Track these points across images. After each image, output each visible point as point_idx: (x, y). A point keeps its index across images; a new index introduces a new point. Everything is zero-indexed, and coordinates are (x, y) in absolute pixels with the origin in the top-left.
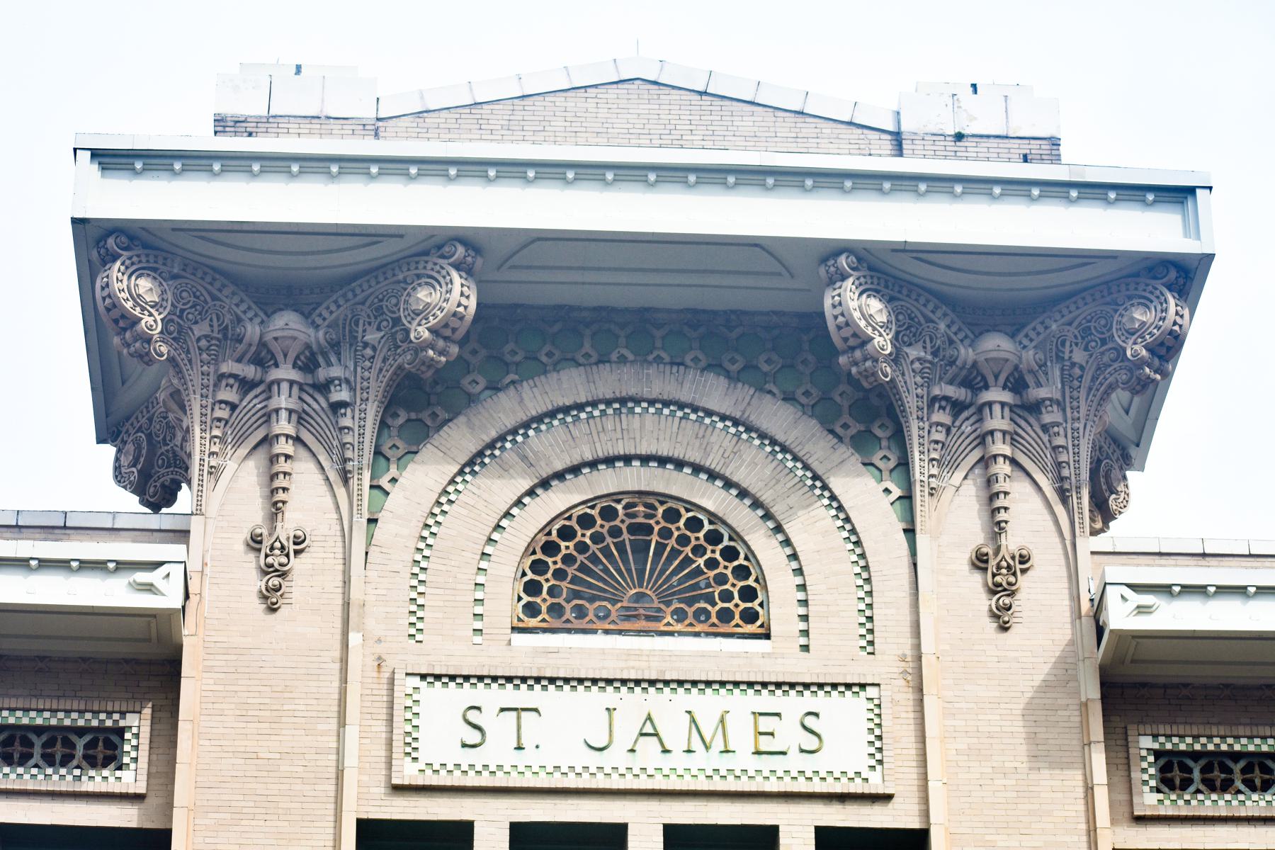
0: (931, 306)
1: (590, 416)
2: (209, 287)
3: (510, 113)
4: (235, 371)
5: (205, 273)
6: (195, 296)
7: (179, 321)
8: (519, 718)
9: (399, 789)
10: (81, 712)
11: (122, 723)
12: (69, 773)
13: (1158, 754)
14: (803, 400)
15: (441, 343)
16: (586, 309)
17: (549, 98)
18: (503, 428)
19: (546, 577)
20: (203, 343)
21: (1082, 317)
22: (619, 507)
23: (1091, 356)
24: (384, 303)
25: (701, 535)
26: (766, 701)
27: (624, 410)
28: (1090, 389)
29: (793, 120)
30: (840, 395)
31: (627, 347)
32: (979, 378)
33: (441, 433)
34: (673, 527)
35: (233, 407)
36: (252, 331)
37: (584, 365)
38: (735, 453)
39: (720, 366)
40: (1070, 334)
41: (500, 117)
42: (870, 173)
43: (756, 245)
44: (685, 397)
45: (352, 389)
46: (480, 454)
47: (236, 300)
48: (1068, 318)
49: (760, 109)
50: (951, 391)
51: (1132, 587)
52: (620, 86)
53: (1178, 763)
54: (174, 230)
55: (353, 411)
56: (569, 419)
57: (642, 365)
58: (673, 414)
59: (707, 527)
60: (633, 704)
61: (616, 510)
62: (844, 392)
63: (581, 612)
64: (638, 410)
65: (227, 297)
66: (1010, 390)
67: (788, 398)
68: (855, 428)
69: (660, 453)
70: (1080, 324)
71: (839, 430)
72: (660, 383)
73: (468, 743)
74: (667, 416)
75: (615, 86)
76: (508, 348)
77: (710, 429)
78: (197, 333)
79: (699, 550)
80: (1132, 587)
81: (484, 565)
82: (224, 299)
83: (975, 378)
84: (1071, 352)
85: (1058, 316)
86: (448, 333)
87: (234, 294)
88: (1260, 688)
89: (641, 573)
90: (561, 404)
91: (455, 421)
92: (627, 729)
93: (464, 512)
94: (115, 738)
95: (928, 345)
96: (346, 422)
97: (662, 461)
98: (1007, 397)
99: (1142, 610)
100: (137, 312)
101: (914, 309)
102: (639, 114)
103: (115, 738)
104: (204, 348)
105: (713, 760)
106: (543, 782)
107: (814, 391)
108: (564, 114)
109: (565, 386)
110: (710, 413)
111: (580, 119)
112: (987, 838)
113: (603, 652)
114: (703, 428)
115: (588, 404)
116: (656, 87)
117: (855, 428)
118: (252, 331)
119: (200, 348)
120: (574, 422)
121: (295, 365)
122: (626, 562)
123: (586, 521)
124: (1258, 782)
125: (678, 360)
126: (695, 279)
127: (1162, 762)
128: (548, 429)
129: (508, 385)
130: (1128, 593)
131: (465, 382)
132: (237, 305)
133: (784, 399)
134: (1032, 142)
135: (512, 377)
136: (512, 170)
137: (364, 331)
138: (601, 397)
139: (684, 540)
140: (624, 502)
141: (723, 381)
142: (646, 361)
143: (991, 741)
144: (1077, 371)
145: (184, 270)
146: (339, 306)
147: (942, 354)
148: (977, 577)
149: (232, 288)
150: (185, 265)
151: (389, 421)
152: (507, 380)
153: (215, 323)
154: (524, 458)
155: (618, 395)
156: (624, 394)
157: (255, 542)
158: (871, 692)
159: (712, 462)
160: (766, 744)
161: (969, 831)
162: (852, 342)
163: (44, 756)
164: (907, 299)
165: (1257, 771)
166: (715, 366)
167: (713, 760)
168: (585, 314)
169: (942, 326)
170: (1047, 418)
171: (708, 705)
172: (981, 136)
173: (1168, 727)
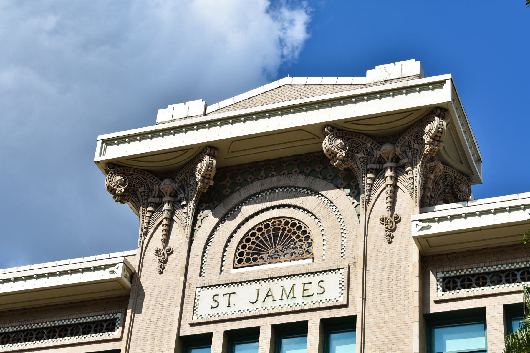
0: (364, 139)
1: (262, 195)
2: (143, 176)
3: (245, 104)
5: (141, 172)
6: (138, 179)
7: (133, 188)
8: (230, 296)
9: (192, 325)
11: (116, 317)
14: (329, 178)
16: (262, 161)
17: (257, 97)
18: (234, 204)
19: (246, 250)
20: (142, 194)
21: (415, 132)
23: (419, 145)
24: (448, 178)
26: (307, 279)
27: (273, 192)
28: (420, 156)
29: (333, 88)
30: (341, 174)
31: (275, 171)
32: (383, 160)
33: (215, 209)
34: (287, 227)
37: (261, 180)
38: (306, 199)
39: (303, 172)
40: (412, 139)
41: (242, 106)
42: (326, 100)
43: (300, 130)
44: (291, 184)
47: (152, 178)
48: (410, 134)
49: (323, 86)
50: (374, 166)
51: (420, 221)
52: (279, 88)
53: (467, 279)
55: (187, 207)
56: (255, 198)
57: (279, 176)
60: (264, 286)
61: (269, 224)
62: (342, 173)
64: (277, 191)
65: (149, 178)
66: (395, 162)
69: (282, 204)
70: (414, 135)
72: (284, 181)
73: (213, 307)
74: (286, 191)
75: (278, 89)
76: (238, 179)
77: (299, 193)
80: (420, 221)
81: (324, 252)
82: (148, 179)
83: (382, 160)
84: (413, 145)
85: (407, 134)
86: (208, 176)
87: (151, 177)
88: (482, 250)
89: (275, 244)
90: (252, 193)
91: (220, 205)
93: (221, 233)
95: (365, 152)
98: (393, 164)
99: (423, 228)
101: (357, 141)
102: (284, 96)
104: (143, 195)
105: (290, 301)
106: (234, 316)
108: (261, 101)
109: (254, 187)
110: (299, 188)
111: (266, 102)
112: (377, 315)
113: (258, 271)
114: (297, 193)
115: (261, 192)
116: (291, 86)
119: (141, 196)
120: (257, 199)
121: (170, 196)
122: (271, 241)
124: (481, 283)
125: (290, 172)
126: (290, 145)
127: (446, 281)
128: (249, 202)
129: (237, 190)
130: (418, 222)
132: (152, 180)
133: (323, 179)
134: (410, 78)
137: (190, 181)
138: (265, 189)
139: (289, 231)
140: (272, 222)
141: (304, 177)
142: (280, 175)
143: (381, 282)
144: (415, 151)
145: (134, 172)
146: (182, 175)
147: (370, 154)
149: (150, 175)
150: (135, 170)
152: (237, 189)
153: (146, 187)
155: (270, 187)
156: (272, 186)
158: (341, 271)
161: (371, 313)
162: (332, 155)
164: (355, 138)
165: (481, 279)
166: (302, 173)
168: (261, 163)
169: (369, 145)
171: (288, 283)
172: (393, 79)
173: (447, 269)
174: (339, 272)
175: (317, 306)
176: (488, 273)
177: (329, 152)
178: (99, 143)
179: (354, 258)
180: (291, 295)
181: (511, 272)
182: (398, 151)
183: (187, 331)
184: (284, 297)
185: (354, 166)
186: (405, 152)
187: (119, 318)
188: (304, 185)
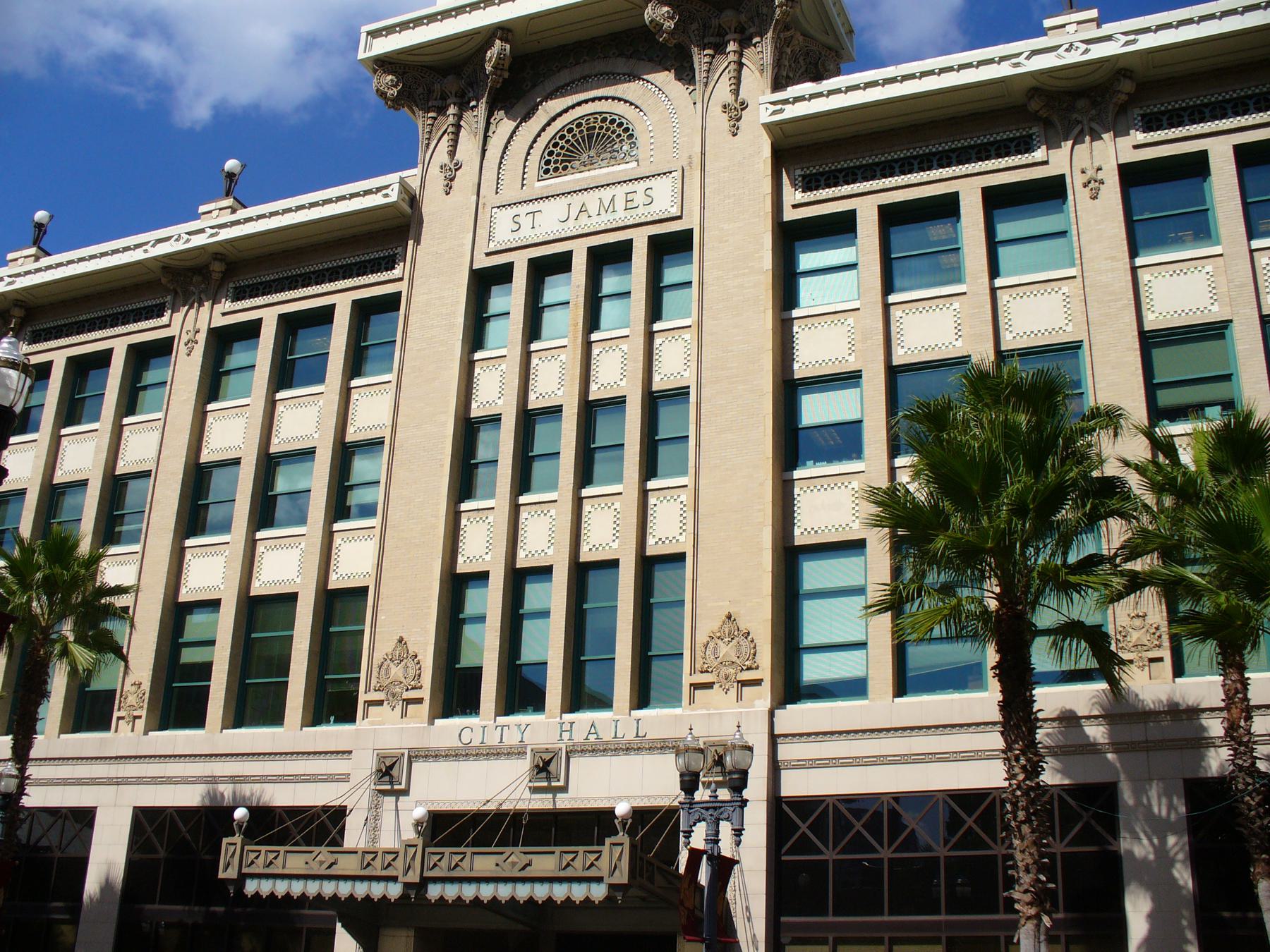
4: (711, 41)
11: (1031, 132)
15: (499, 72)
20: (421, 97)
22: (583, 122)
25: (607, 123)
36: (715, 22)
44: (608, 70)
50: (712, 39)
51: (771, 103)
58: (604, 78)
59: (574, 126)
60: (577, 200)
63: (565, 168)
78: (693, 29)
80: (771, 103)
92: (574, 211)
99: (775, 113)
100: (386, 90)
105: (610, 216)
115: (570, 83)
123: (570, 130)
127: (1146, 119)
135: (541, 79)
136: (404, 26)
139: (608, 129)
148: (726, 115)
160: (630, 205)
166: (621, 55)
167: (610, 216)
171: (606, 194)
174: (671, 176)
175: (643, 220)
177: (653, 24)
178: (363, 36)
179: (690, 157)
180: (611, 209)
182: (743, 18)
183: (482, 262)
186: (751, 19)
188: (625, 71)
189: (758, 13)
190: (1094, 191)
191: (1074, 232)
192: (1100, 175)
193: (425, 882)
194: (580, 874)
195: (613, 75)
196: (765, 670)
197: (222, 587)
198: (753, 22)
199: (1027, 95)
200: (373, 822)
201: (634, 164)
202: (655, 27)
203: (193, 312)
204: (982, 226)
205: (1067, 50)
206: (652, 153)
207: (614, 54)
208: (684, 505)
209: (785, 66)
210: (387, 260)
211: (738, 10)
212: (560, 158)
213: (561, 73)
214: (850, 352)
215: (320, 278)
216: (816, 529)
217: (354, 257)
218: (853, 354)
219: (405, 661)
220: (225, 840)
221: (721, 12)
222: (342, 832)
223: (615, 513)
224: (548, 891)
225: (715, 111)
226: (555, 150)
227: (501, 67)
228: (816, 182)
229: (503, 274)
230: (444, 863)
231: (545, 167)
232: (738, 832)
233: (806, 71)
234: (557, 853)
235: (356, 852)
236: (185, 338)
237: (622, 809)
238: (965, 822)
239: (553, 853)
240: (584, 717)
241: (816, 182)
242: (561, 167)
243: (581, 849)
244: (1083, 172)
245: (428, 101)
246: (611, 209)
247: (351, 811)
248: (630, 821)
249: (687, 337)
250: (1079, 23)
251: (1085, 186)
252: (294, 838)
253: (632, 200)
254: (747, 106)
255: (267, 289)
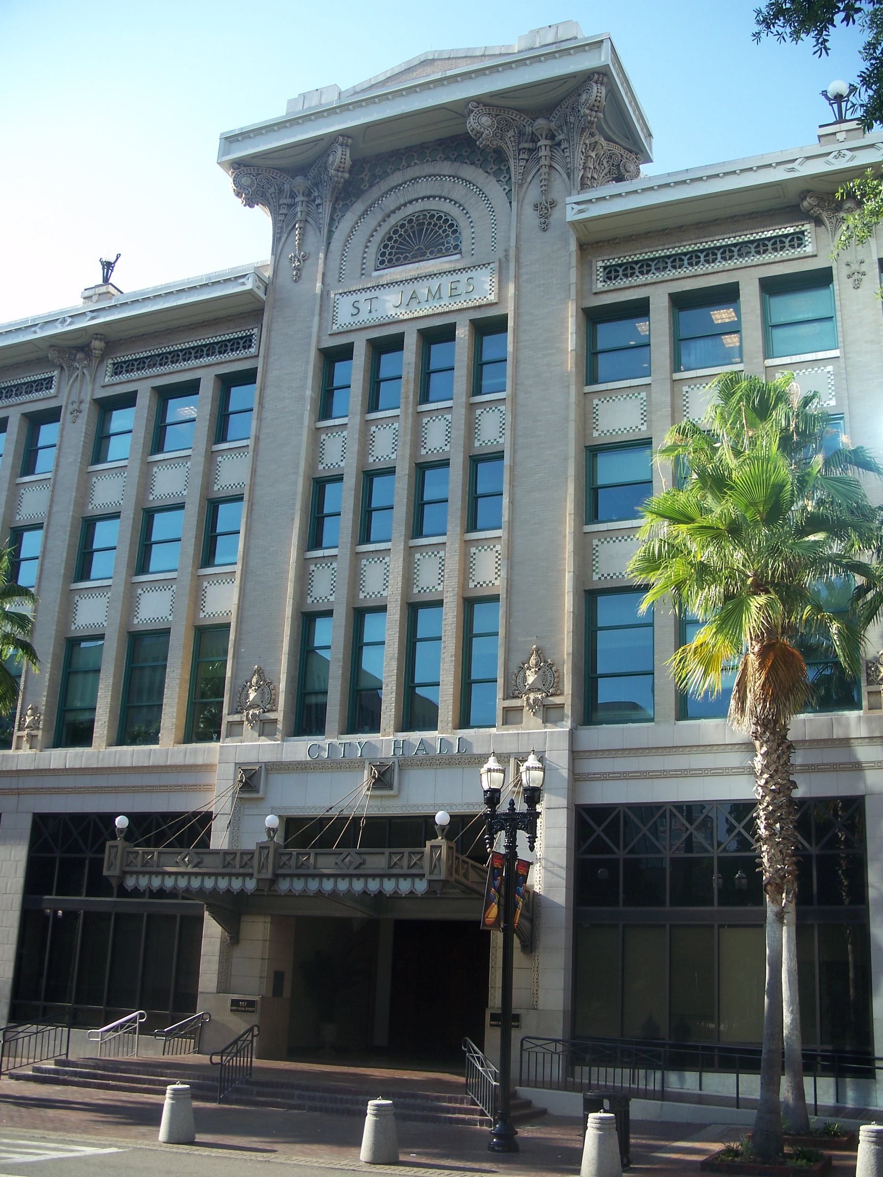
0: (514, 115)
10: (641, 254)
11: (803, 229)
12: (749, 258)
13: (605, 268)
22: (414, 218)
25: (435, 219)
35: (286, 215)
36: (528, 130)
45: (322, 199)
46: (367, 211)
50: (526, 145)
54: (491, 96)
58: (427, 180)
60: (409, 289)
63: (398, 259)
67: (472, 163)
68: (495, 168)
71: (489, 171)
72: (427, 169)
79: (440, 227)
89: (420, 242)
94: (800, 236)
96: (320, 210)
97: (429, 197)
98: (548, 142)
99: (580, 211)
103: (800, 236)
107: (481, 158)
110: (445, 176)
115: (402, 183)
117: (495, 168)
118: (528, 130)
123: (403, 226)
131: (362, 187)
135: (378, 180)
139: (435, 225)
151: (336, 206)
154: (381, 208)
157: (536, 206)
159: (444, 194)
163: (738, 255)
166: (447, 158)
170: (562, 147)
171: (434, 283)
176: (652, 260)
180: (437, 296)
181: (795, 236)
184: (430, 299)
185: (504, 146)
186: (560, 127)
187: (808, 231)
189: (566, 122)
190: (857, 282)
191: (839, 318)
192: (863, 268)
193: (276, 877)
194: (405, 871)
195: (440, 176)
196: (566, 698)
197: (105, 624)
198: (562, 130)
199: (800, 196)
200: (234, 825)
201: (458, 257)
202: (476, 135)
203: (75, 390)
204: (759, 312)
205: (836, 157)
206: (473, 247)
207: (441, 157)
208: (499, 554)
209: (590, 168)
210: (184, 352)
211: (548, 119)
212: (393, 251)
213: (395, 175)
214: (643, 421)
215: (187, 354)
216: (611, 575)
217: (216, 337)
218: (645, 424)
219: (543, 669)
220: (108, 844)
221: (534, 121)
222: (208, 834)
223: (441, 560)
224: (378, 886)
225: (529, 211)
226: (389, 243)
227: (596, 109)
228: (696, 258)
229: (345, 353)
230: (293, 862)
231: (381, 259)
232: (532, 840)
233: (609, 172)
234: (387, 854)
235: (219, 853)
236: (71, 408)
237: (442, 818)
238: (594, 831)
239: (384, 853)
240: (415, 736)
241: (696, 258)
242: (394, 258)
243: (406, 850)
244: (848, 265)
245: (279, 199)
246: (437, 296)
247: (215, 817)
248: (447, 828)
249: (502, 408)
250: (847, 131)
251: (849, 277)
252: (137, 840)
253: (456, 289)
254: (556, 205)
255: (141, 364)
